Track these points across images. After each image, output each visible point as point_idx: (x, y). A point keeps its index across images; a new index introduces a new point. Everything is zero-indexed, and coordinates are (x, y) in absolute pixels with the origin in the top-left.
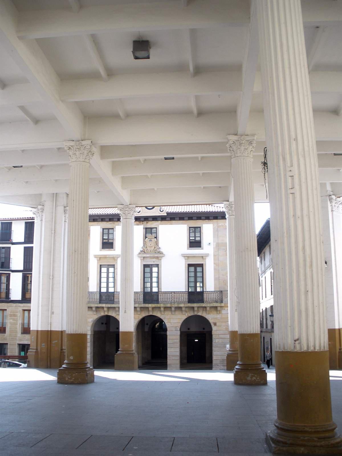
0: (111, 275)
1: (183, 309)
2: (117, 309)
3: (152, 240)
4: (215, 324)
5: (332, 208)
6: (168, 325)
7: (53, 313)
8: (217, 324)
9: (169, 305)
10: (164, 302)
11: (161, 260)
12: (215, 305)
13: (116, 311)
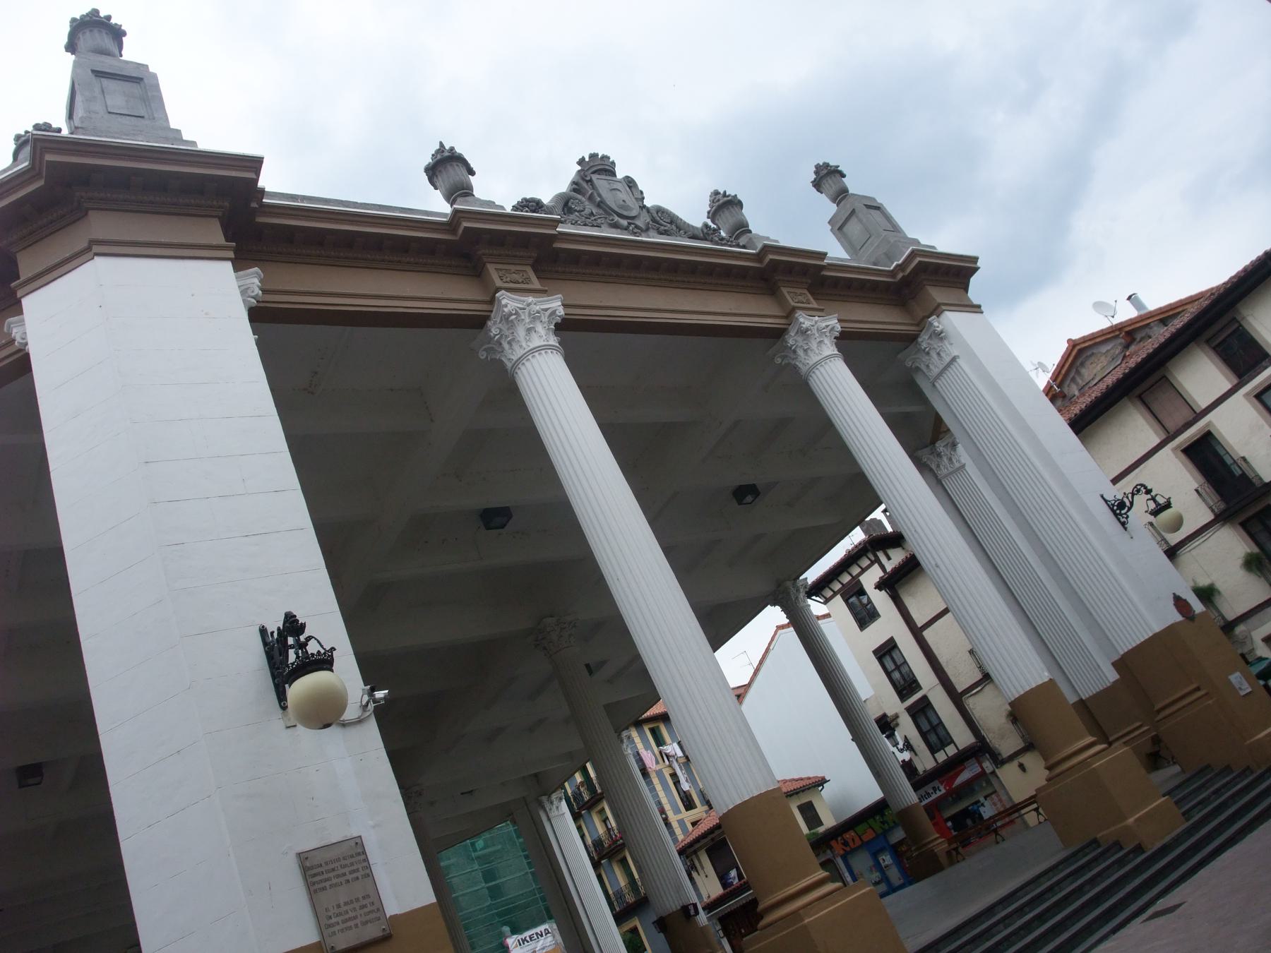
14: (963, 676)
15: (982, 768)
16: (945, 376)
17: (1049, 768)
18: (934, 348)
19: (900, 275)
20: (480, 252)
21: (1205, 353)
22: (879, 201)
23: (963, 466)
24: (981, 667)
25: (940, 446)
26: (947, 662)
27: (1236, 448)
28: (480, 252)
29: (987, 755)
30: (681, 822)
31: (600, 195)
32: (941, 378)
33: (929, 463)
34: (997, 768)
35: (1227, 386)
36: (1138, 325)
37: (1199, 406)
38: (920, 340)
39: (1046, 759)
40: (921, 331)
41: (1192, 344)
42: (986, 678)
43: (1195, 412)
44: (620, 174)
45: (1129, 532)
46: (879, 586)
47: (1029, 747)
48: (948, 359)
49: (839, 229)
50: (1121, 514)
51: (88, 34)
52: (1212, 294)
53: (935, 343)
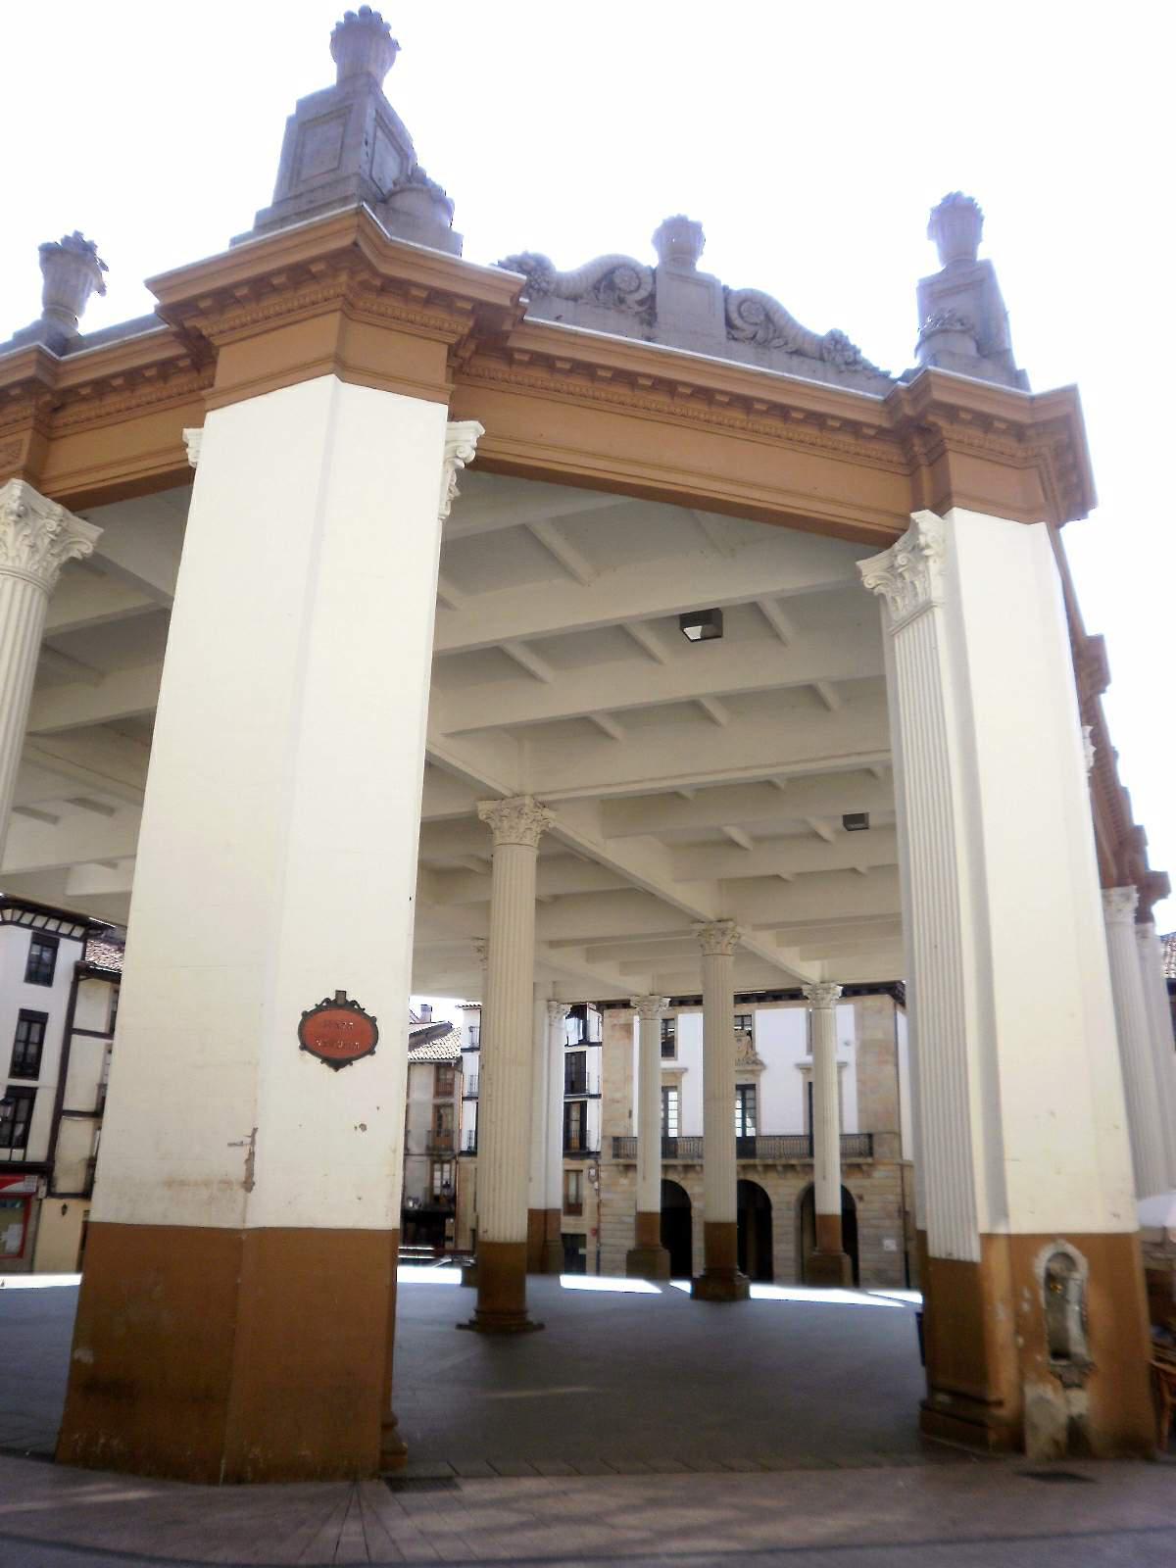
0: (672, 1105)
1: (799, 1168)
2: (698, 1168)
3: (743, 1038)
4: (861, 1198)
5: (550, 1021)
6: (774, 1199)
7: (530, 1179)
8: (866, 1198)
9: (770, 1162)
10: (763, 1157)
11: (759, 1076)
12: (860, 1160)
13: (697, 1173)
14: (79, 1097)
16: (915, 626)
22: (104, 280)
42: (97, 1114)
51: (508, 1235)
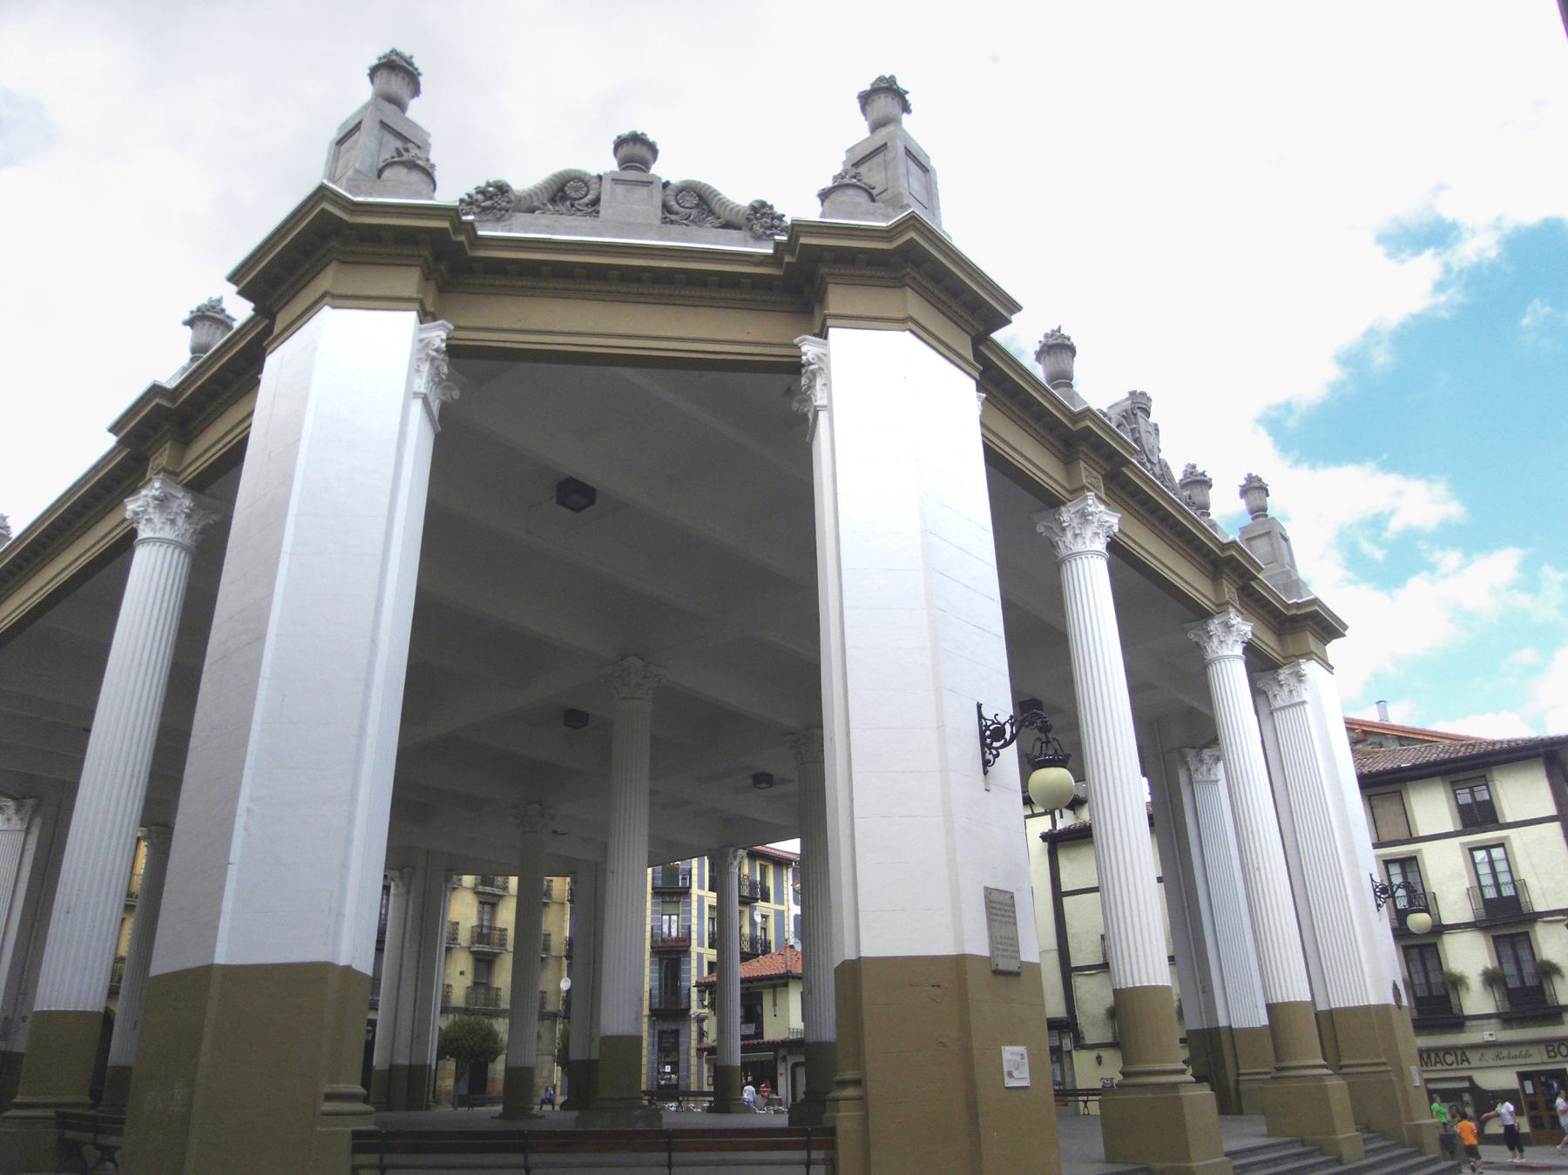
14: (1083, 953)
15: (1061, 1042)
17: (1125, 1074)
18: (1289, 685)
19: (1294, 612)
20: (1081, 448)
21: (1445, 791)
23: (1217, 781)
24: (1105, 955)
25: (1206, 753)
26: (1074, 934)
27: (1432, 883)
28: (1081, 448)
29: (1071, 1034)
30: (700, 956)
31: (1139, 432)
32: (1283, 712)
33: (1190, 762)
34: (1075, 1050)
35: (1450, 828)
36: (1375, 730)
37: (1417, 832)
38: (1280, 671)
39: (1125, 1063)
40: (1284, 665)
41: (1439, 778)
42: (1105, 967)
43: (1411, 835)
44: (1152, 420)
45: (1380, 914)
46: (1044, 837)
47: (1114, 1045)
48: (1297, 700)
49: (1247, 539)
50: (1380, 897)
52: (1473, 745)
53: (1293, 681)
